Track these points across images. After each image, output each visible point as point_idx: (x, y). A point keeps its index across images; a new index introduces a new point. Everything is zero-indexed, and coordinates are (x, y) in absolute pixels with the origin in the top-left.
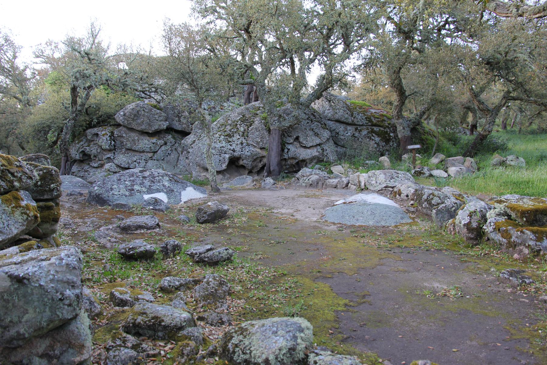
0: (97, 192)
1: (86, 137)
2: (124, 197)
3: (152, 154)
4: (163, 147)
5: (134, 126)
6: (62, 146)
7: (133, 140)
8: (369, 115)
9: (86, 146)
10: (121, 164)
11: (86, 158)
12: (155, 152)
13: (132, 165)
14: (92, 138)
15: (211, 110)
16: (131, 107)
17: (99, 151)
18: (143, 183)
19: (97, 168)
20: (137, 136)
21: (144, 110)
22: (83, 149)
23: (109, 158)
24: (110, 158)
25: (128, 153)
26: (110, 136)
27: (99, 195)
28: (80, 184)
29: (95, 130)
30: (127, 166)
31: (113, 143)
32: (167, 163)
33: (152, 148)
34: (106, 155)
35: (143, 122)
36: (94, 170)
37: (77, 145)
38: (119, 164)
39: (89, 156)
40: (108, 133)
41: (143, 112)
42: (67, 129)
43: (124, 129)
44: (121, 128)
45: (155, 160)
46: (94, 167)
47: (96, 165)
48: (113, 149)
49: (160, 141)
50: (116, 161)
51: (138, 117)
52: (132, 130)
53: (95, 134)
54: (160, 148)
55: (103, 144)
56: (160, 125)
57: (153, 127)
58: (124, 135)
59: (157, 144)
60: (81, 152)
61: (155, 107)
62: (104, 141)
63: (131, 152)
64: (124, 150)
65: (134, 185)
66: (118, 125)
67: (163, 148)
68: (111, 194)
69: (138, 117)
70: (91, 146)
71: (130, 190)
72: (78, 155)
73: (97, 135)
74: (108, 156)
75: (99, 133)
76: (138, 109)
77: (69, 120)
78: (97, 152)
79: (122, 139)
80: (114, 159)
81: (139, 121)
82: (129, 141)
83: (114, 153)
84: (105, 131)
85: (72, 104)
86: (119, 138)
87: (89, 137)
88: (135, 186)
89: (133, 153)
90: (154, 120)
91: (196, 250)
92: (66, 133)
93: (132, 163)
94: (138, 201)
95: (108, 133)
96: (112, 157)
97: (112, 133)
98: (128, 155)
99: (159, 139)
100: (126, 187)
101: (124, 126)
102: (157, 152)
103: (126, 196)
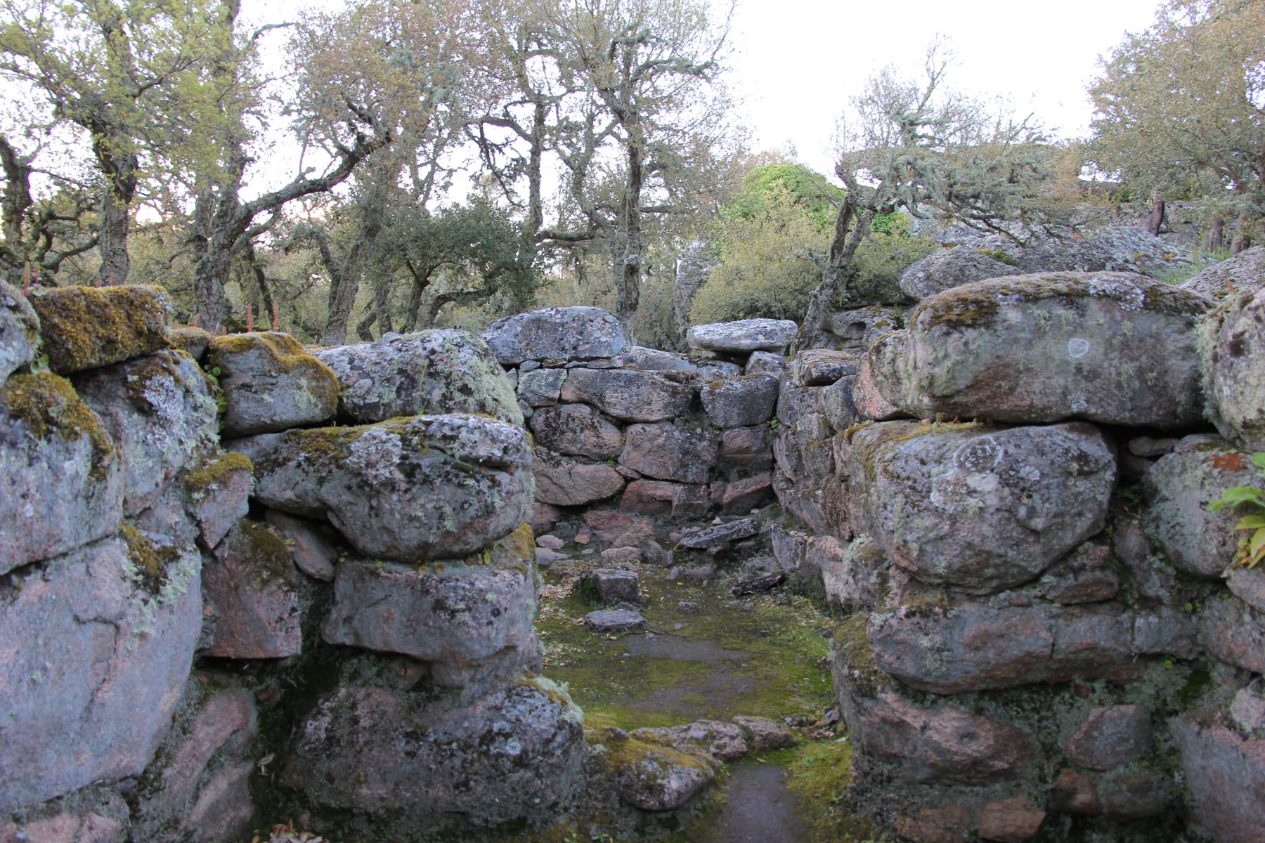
8: (97, 820)
15: (1143, 263)
41: (974, 271)
42: (817, 308)
53: (854, 324)
73: (861, 326)
75: (867, 321)
76: (961, 263)
87: (840, 332)
92: (815, 318)
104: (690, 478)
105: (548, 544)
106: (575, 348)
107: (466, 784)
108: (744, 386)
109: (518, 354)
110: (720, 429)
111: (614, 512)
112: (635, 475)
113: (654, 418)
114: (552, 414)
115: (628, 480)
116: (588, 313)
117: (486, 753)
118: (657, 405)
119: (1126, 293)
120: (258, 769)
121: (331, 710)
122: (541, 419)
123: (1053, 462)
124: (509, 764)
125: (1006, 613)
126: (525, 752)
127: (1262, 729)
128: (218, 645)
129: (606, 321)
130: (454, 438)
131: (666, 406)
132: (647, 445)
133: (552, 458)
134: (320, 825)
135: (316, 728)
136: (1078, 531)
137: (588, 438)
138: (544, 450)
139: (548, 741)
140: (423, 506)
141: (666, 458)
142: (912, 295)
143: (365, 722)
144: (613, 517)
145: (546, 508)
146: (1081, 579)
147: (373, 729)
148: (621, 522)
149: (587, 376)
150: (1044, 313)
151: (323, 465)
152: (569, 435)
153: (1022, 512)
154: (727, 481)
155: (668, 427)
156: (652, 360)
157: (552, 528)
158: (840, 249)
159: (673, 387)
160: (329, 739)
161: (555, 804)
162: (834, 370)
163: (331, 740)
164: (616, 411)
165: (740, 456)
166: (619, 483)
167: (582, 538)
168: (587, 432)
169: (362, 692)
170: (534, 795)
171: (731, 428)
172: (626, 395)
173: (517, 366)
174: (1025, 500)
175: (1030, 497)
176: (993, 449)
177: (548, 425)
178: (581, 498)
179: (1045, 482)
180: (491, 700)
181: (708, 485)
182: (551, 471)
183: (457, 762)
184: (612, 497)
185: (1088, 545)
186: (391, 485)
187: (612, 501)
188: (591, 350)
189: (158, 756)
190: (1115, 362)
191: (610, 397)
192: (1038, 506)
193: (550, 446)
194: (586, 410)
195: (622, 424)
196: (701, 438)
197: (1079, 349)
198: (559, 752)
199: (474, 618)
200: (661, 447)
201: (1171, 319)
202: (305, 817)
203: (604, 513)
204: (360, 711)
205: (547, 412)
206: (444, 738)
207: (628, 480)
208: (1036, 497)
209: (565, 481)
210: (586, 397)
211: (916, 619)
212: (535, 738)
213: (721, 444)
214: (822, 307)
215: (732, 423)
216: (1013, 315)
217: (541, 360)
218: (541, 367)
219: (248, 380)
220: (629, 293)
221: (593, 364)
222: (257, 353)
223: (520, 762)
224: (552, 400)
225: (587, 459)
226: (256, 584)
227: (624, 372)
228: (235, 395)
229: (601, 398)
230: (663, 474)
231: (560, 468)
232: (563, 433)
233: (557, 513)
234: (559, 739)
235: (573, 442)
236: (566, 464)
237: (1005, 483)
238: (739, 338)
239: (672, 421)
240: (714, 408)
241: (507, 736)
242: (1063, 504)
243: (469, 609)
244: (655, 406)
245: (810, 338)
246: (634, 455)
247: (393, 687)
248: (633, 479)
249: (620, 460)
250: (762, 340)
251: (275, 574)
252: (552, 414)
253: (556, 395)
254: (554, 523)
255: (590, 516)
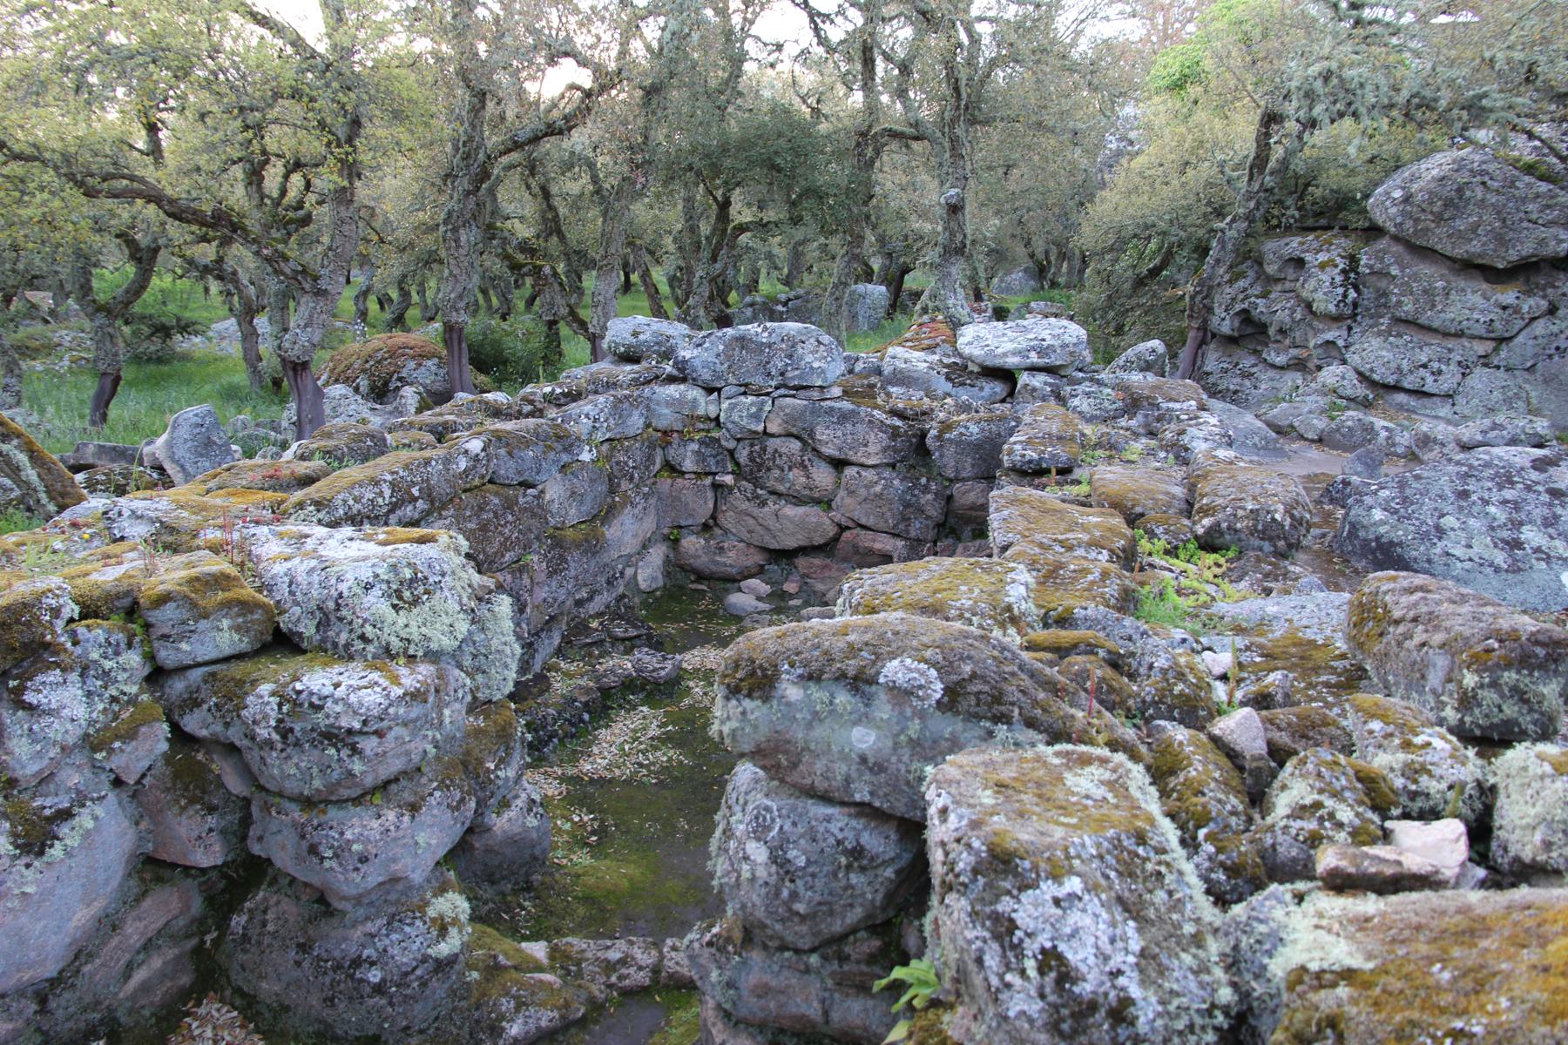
0: (1382, 530)
1: (1260, 264)
2: (1489, 570)
3: (1490, 345)
4: (1541, 322)
5: (1439, 239)
6: (1199, 298)
7: (1425, 292)
9: (1257, 297)
10: (1372, 370)
11: (1249, 330)
12: (1502, 340)
13: (1411, 378)
14: (1280, 270)
16: (1435, 172)
17: (1298, 316)
18: (1556, 517)
19: (1282, 368)
20: (1442, 277)
21: (1484, 183)
22: (1246, 305)
23: (1330, 344)
24: (1333, 343)
25: (1399, 335)
26: (1344, 271)
27: (1391, 543)
28: (1256, 439)
29: (1293, 245)
30: (1391, 380)
31: (1352, 294)
32: (1546, 381)
33: (1497, 325)
34: (1323, 331)
35: (1474, 229)
36: (1271, 373)
37: (1228, 290)
38: (1365, 368)
39: (1262, 328)
40: (1338, 260)
42: (1223, 248)
43: (1397, 248)
44: (1383, 243)
45: (1498, 367)
46: (1273, 366)
47: (1280, 360)
48: (1348, 316)
49: (1532, 301)
50: (1356, 357)
51: (1457, 208)
52: (1425, 253)
53: (1291, 259)
54: (1527, 325)
55: (1319, 295)
56: (1542, 242)
57: (1514, 247)
58: (1394, 271)
59: (1517, 310)
60: (1237, 314)
61: (1530, 169)
62: (1323, 288)
63: (1412, 330)
64: (1385, 321)
65: (1521, 524)
66: (1374, 231)
67: (1540, 328)
68: (1438, 551)
69: (1457, 208)
70: (1273, 296)
71: (1507, 543)
72: (1227, 322)
73: (1299, 263)
74: (1329, 336)
75: (1308, 257)
76: (1463, 177)
77: (1233, 220)
78: (1293, 320)
79: (1383, 284)
80: (1346, 347)
81: (1460, 225)
82: (1412, 293)
83: (1350, 329)
84: (1328, 251)
85: (1251, 169)
86: (1374, 278)
87: (1271, 269)
88: (1524, 529)
89: (1419, 337)
90: (1521, 220)
91: (1411, 591)
92: (1218, 261)
93: (1411, 372)
94: (1544, 599)
95: (1338, 260)
96: (1341, 343)
97: (1353, 260)
98: (1400, 342)
99: (1529, 293)
100: (1492, 529)
101: (1396, 239)
102: (1511, 339)
103: (1497, 570)
104: (913, 534)
105: (752, 590)
106: (782, 374)
107: (332, 1000)
108: (983, 430)
109: (719, 378)
110: (951, 480)
111: (828, 561)
112: (851, 524)
113: (870, 462)
114: (757, 448)
115: (842, 529)
116: (799, 332)
117: (352, 976)
118: (874, 449)
119: (920, 687)
120: (203, 942)
121: (250, 910)
122: (745, 453)
123: (822, 851)
124: (368, 990)
125: (786, 973)
126: (383, 980)
127: (1340, 1037)
128: (155, 850)
129: (820, 343)
130: (321, 708)
131: (885, 450)
132: (863, 492)
133: (758, 497)
134: (238, 1002)
135: (238, 921)
136: (848, 921)
137: (796, 477)
138: (750, 486)
139: (406, 974)
140: (297, 765)
141: (885, 509)
142: (1380, 222)
143: (270, 928)
144: (826, 566)
145: (752, 550)
146: (846, 968)
147: (274, 935)
148: (834, 573)
149: (794, 408)
150: (825, 696)
151: (228, 711)
152: (776, 473)
153: (785, 893)
154: (959, 539)
155: (887, 473)
156: (901, 371)
157: (760, 572)
158: (1262, 169)
159: (895, 428)
160: (244, 935)
161: (407, 1028)
162: (1030, 462)
163: (245, 938)
164: (829, 450)
165: (974, 513)
166: (832, 531)
167: (791, 587)
168: (795, 471)
169: (275, 899)
170: (385, 1020)
171: (963, 480)
172: (839, 433)
173: (719, 390)
174: (788, 884)
175: (792, 881)
176: (773, 820)
177: (752, 460)
178: (791, 543)
179: (811, 870)
180: (370, 927)
181: (935, 543)
182: (756, 511)
183: (327, 980)
184: (826, 544)
185: (862, 934)
186: (270, 744)
187: (826, 549)
188: (800, 377)
189: (76, 957)
190: (905, 758)
191: (822, 433)
192: (801, 890)
193: (756, 483)
194: (796, 445)
195: (839, 464)
196: (926, 489)
197: (864, 739)
198: (415, 984)
199: (341, 864)
200: (879, 496)
201: (970, 725)
202: (228, 993)
203: (817, 561)
204: (270, 916)
205: (752, 445)
206: (324, 955)
207: (842, 529)
208: (799, 883)
209: (771, 523)
210: (794, 430)
211: (713, 950)
212: (395, 970)
213: (950, 498)
214: (1230, 246)
215: (964, 474)
216: (792, 692)
217: (746, 385)
218: (745, 393)
219: (166, 631)
220: (952, 234)
221: (802, 393)
222: (174, 605)
223: (379, 989)
224: (756, 432)
225: (798, 500)
226: (176, 809)
227: (838, 405)
228: (156, 644)
229: (812, 434)
230: (882, 525)
231: (766, 509)
232: (769, 469)
233: (766, 556)
234: (419, 972)
235: (781, 480)
236: (772, 505)
237: (773, 859)
238: (1005, 355)
239: (893, 466)
240: (941, 456)
241: (372, 964)
242: (830, 894)
243: (336, 855)
244: (872, 449)
245: (1211, 288)
246: (848, 501)
247: (298, 899)
248: (848, 528)
249: (834, 505)
250: (1034, 358)
251: (192, 801)
252: (757, 448)
253: (760, 428)
254: (762, 566)
255: (801, 562)
